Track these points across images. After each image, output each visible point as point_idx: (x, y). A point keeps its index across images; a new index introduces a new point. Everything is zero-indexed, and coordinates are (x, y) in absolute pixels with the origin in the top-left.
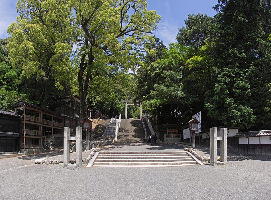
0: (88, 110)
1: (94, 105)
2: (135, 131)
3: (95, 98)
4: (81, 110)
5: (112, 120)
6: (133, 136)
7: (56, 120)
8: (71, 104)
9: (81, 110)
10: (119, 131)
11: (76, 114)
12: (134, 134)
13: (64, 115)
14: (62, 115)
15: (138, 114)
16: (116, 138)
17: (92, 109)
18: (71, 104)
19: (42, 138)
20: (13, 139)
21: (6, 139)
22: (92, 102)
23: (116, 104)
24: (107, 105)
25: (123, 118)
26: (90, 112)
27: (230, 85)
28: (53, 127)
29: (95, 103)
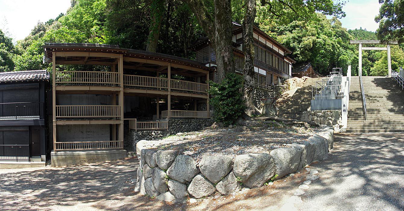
0: (284, 61)
1: (298, 54)
2: (389, 98)
3: (300, 42)
4: (217, 26)
5: (332, 78)
6: (391, 110)
7: (199, 79)
8: (241, 45)
9: (217, 26)
10: (351, 98)
11: (254, 67)
12: (390, 104)
13: (212, 65)
14: (207, 65)
15: (379, 71)
16: (345, 115)
17: (295, 60)
18: (241, 45)
19: (122, 122)
20: (16, 129)
21: (3, 131)
22: (293, 49)
23: (339, 55)
24: (324, 56)
25: (355, 72)
26: (290, 66)
27: (276, 114)
28: (169, 93)
29: (300, 49)
